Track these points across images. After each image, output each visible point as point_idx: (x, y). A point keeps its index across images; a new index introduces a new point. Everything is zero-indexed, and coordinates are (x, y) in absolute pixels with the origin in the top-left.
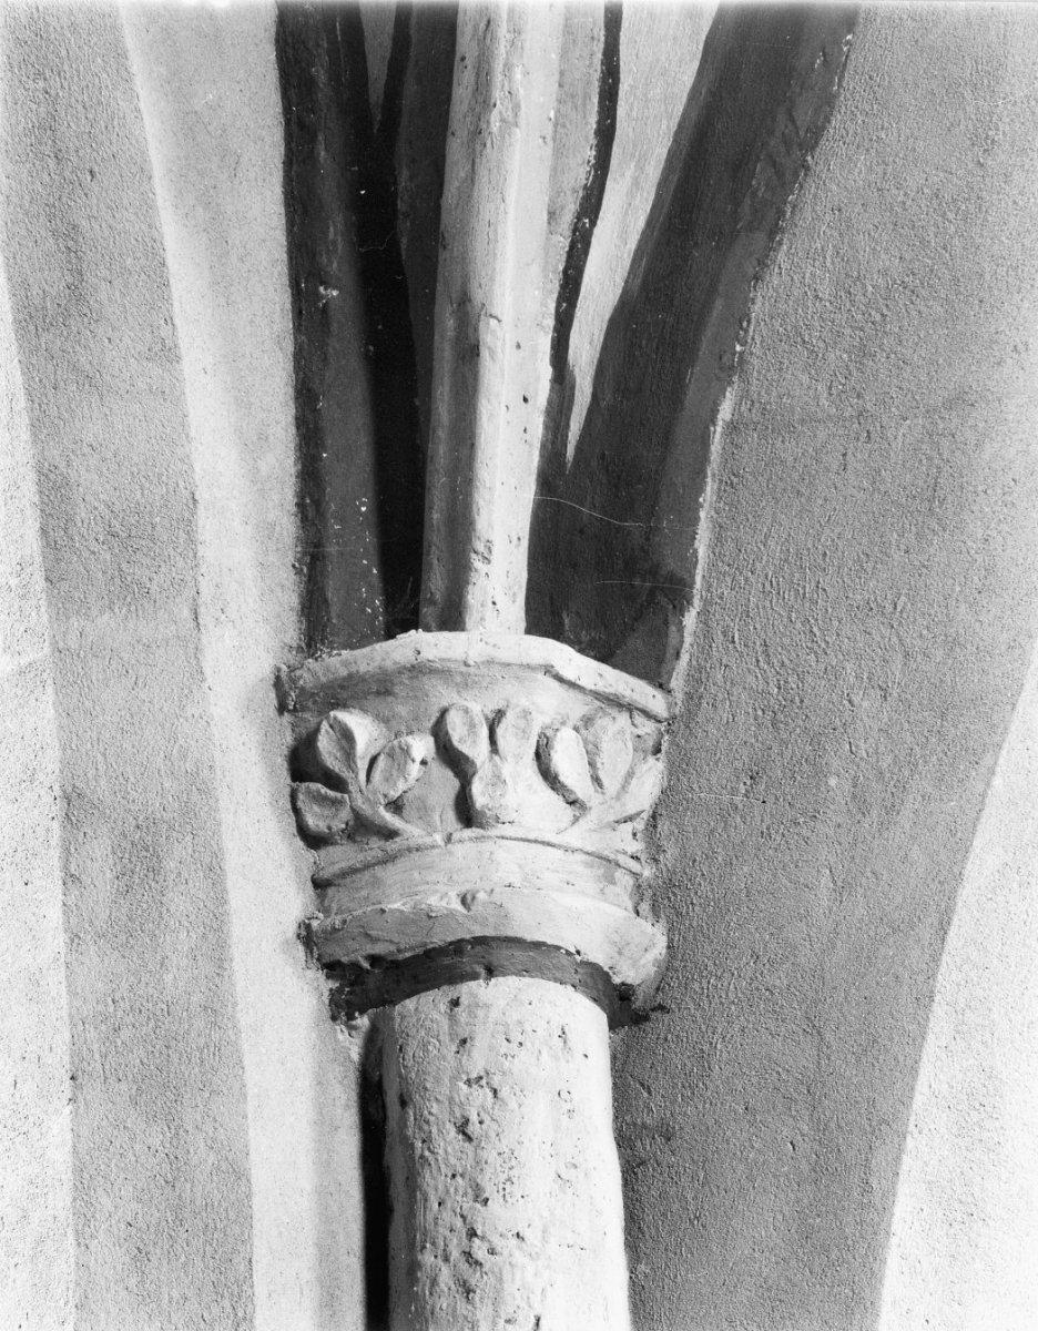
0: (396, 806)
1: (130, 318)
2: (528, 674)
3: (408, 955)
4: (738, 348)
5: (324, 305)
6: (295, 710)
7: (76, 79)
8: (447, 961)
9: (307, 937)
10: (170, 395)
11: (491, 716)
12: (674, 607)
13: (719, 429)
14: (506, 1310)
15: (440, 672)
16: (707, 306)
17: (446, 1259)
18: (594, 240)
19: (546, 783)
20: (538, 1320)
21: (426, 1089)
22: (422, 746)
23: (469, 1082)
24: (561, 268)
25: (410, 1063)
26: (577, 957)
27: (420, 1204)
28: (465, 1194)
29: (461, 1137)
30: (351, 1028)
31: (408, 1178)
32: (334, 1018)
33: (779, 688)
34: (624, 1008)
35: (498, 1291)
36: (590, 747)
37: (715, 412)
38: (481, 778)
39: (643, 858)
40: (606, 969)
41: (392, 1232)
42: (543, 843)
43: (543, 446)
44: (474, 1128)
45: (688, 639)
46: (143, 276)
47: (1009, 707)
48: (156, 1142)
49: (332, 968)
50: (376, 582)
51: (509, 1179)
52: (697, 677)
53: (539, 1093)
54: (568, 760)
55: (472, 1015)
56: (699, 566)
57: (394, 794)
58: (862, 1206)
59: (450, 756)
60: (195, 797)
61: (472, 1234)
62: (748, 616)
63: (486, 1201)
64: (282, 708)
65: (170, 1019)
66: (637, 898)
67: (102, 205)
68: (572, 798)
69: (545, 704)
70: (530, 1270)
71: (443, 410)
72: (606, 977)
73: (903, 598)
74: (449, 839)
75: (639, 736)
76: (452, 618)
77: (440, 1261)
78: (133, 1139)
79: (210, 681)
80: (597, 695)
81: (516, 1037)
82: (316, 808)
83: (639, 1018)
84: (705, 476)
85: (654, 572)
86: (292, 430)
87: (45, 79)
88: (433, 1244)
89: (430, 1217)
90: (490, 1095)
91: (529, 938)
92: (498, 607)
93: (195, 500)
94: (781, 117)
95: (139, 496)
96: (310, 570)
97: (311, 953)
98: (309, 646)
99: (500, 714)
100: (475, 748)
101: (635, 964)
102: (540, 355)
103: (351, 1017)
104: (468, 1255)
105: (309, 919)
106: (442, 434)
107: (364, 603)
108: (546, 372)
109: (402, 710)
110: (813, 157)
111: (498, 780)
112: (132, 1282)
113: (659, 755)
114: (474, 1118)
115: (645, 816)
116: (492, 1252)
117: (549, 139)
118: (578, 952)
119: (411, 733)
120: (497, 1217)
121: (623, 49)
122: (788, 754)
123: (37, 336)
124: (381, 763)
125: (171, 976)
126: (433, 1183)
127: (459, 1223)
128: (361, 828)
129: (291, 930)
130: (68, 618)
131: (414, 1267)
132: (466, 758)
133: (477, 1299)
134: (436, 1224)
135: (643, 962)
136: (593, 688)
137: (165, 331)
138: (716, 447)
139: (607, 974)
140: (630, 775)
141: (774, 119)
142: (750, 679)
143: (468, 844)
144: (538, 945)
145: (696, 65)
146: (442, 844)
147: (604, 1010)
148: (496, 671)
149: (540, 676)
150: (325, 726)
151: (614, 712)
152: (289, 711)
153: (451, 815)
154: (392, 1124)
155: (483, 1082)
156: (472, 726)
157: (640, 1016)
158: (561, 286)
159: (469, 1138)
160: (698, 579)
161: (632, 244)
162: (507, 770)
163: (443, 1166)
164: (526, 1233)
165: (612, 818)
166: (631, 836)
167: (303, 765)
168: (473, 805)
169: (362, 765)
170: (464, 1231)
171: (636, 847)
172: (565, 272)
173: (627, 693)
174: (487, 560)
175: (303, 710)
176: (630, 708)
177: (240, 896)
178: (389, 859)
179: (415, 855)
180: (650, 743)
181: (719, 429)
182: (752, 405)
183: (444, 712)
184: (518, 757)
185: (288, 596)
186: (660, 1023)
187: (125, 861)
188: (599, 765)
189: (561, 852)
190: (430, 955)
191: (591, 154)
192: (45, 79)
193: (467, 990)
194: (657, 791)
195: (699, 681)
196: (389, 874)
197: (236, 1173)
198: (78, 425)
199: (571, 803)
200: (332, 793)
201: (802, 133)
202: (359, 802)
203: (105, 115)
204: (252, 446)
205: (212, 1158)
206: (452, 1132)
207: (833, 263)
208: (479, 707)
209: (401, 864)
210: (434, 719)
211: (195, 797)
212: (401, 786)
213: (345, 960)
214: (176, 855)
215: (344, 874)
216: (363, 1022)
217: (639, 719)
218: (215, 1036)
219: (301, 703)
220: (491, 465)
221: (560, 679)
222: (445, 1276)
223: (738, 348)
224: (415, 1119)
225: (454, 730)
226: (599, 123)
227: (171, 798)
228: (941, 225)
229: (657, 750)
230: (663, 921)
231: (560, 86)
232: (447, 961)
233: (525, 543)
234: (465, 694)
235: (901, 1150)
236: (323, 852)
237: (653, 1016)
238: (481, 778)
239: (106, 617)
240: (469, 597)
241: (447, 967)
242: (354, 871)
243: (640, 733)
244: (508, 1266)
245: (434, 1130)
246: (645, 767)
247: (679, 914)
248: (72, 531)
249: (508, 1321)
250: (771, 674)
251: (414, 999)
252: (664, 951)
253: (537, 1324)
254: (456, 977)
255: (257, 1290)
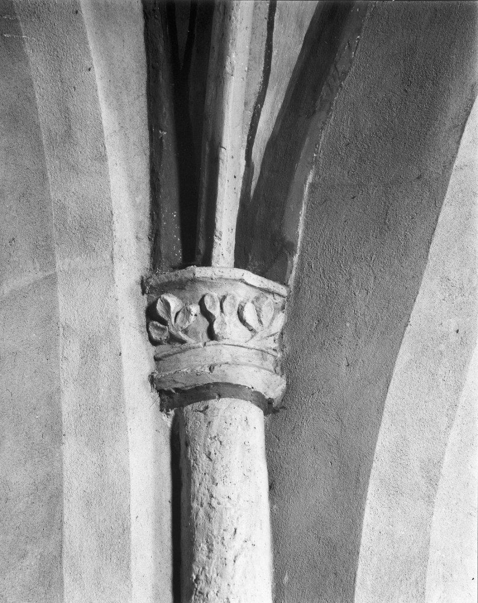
0: (186, 331)
1: (88, 144)
2: (235, 282)
3: (189, 388)
4: (315, 155)
5: (161, 137)
6: (148, 293)
7: (69, 52)
8: (204, 391)
9: (152, 380)
10: (103, 174)
11: (221, 298)
12: (290, 254)
13: (307, 186)
14: (224, 526)
15: (203, 282)
16: (303, 140)
17: (202, 506)
18: (262, 113)
19: (243, 320)
20: (236, 530)
21: (195, 440)
22: (195, 309)
23: (211, 438)
24: (250, 123)
25: (190, 430)
26: (252, 389)
27: (192, 484)
28: (209, 481)
29: (208, 459)
30: (168, 415)
31: (188, 474)
32: (161, 411)
33: (329, 287)
34: (268, 407)
35: (221, 518)
36: (258, 309)
37: (306, 179)
38: (217, 322)
39: (278, 350)
40: (263, 394)
41: (182, 493)
42: (240, 346)
43: (242, 191)
44: (213, 456)
45: (295, 266)
46: (94, 128)
47: (413, 300)
48: (94, 460)
49: (161, 392)
50: (180, 244)
51: (226, 476)
52: (298, 281)
53: (238, 444)
54: (249, 315)
55: (213, 412)
56: (300, 238)
57: (184, 327)
58: (356, 488)
59: (206, 313)
60: (111, 328)
61: (212, 496)
62: (317, 258)
63: (217, 484)
64: (143, 293)
65: (101, 412)
66: (275, 365)
67: (78, 100)
68: (251, 328)
69: (241, 293)
70: (233, 511)
71: (205, 180)
72: (263, 396)
73: (374, 256)
74: (205, 344)
75: (276, 303)
76: (207, 261)
77: (200, 507)
78: (86, 458)
79: (117, 283)
80: (261, 289)
81: (229, 421)
82: (156, 331)
83: (275, 411)
84: (302, 204)
85: (283, 239)
86: (149, 186)
87: (57, 52)
88: (197, 500)
89: (196, 490)
90: (219, 443)
91: (234, 383)
92: (224, 256)
93: (112, 214)
94: (332, 69)
95: (91, 213)
96: (155, 240)
97: (153, 386)
98: (154, 268)
99: (224, 297)
100: (216, 312)
101: (274, 391)
102: (241, 157)
103: (168, 411)
104: (210, 504)
105: (152, 373)
106: (204, 190)
107: (175, 252)
108: (243, 162)
109: (188, 295)
110: (344, 83)
111: (223, 323)
112: (85, 514)
113: (284, 310)
114: (213, 452)
115: (279, 333)
116: (219, 504)
117: (245, 78)
118: (253, 388)
119: (191, 304)
120: (220, 491)
121: (274, 39)
122: (332, 312)
123: (53, 150)
124: (180, 315)
125: (101, 396)
126: (197, 476)
127: (207, 492)
128: (173, 339)
129: (146, 378)
130: (64, 259)
131: (190, 508)
132: (211, 314)
133: (213, 521)
134: (198, 492)
135: (277, 390)
136: (259, 286)
137: (102, 149)
138: (306, 190)
139: (263, 395)
140: (273, 319)
141: (330, 69)
142: (318, 283)
143: (212, 347)
144: (237, 386)
145: (301, 46)
146: (202, 346)
147: (262, 409)
148: (223, 282)
149: (239, 283)
150: (159, 301)
151: (268, 295)
152: (146, 294)
153: (205, 335)
154: (182, 452)
155: (216, 439)
156: (214, 302)
157: (276, 410)
158: (250, 130)
159: (211, 460)
160: (299, 243)
161: (276, 114)
162: (226, 319)
163: (201, 470)
164: (231, 496)
165: (266, 335)
166: (273, 341)
167: (151, 314)
168: (214, 332)
169: (173, 316)
170: (209, 495)
171: (275, 345)
172: (251, 125)
173: (272, 288)
174: (220, 239)
175: (151, 293)
176: (273, 293)
177: (127, 364)
178: (184, 351)
179: (192, 350)
180: (280, 305)
181: (307, 186)
182: (320, 177)
183: (204, 296)
184: (231, 314)
185: (146, 249)
186: (283, 413)
187: (85, 352)
188: (261, 316)
189: (247, 349)
190: (197, 388)
191: (261, 80)
192: (57, 52)
193: (211, 403)
194: (283, 324)
195: (299, 282)
196: (183, 357)
197: (126, 473)
198: (68, 184)
199: (251, 330)
200: (161, 326)
201: (340, 74)
202: (172, 330)
203: (80, 66)
204: (133, 192)
205: (115, 466)
206: (204, 457)
207: (351, 124)
208: (216, 294)
209: (188, 353)
210: (199, 299)
211: (111, 328)
212: (187, 324)
213: (165, 389)
214: (104, 349)
215: (166, 356)
216: (172, 412)
217: (277, 297)
218: (117, 419)
219: (151, 289)
220: (222, 203)
221: (247, 284)
222: (201, 513)
223: (315, 155)
224: (191, 451)
225: (207, 303)
226: (264, 68)
227: (102, 328)
228: (391, 113)
229: (283, 308)
230: (284, 377)
231: (250, 54)
232: (204, 391)
233: (234, 231)
234: (211, 290)
235: (371, 467)
236: (158, 347)
237: (281, 410)
238: (217, 322)
239: (78, 259)
240: (213, 253)
241: (203, 393)
242: (169, 355)
243: (277, 302)
244: (225, 509)
245: (198, 456)
246: (279, 316)
247: (291, 372)
248: (66, 225)
249: (224, 530)
250: (325, 281)
251: (192, 405)
252: (285, 386)
253: (235, 531)
254: (206, 397)
255: (132, 516)
